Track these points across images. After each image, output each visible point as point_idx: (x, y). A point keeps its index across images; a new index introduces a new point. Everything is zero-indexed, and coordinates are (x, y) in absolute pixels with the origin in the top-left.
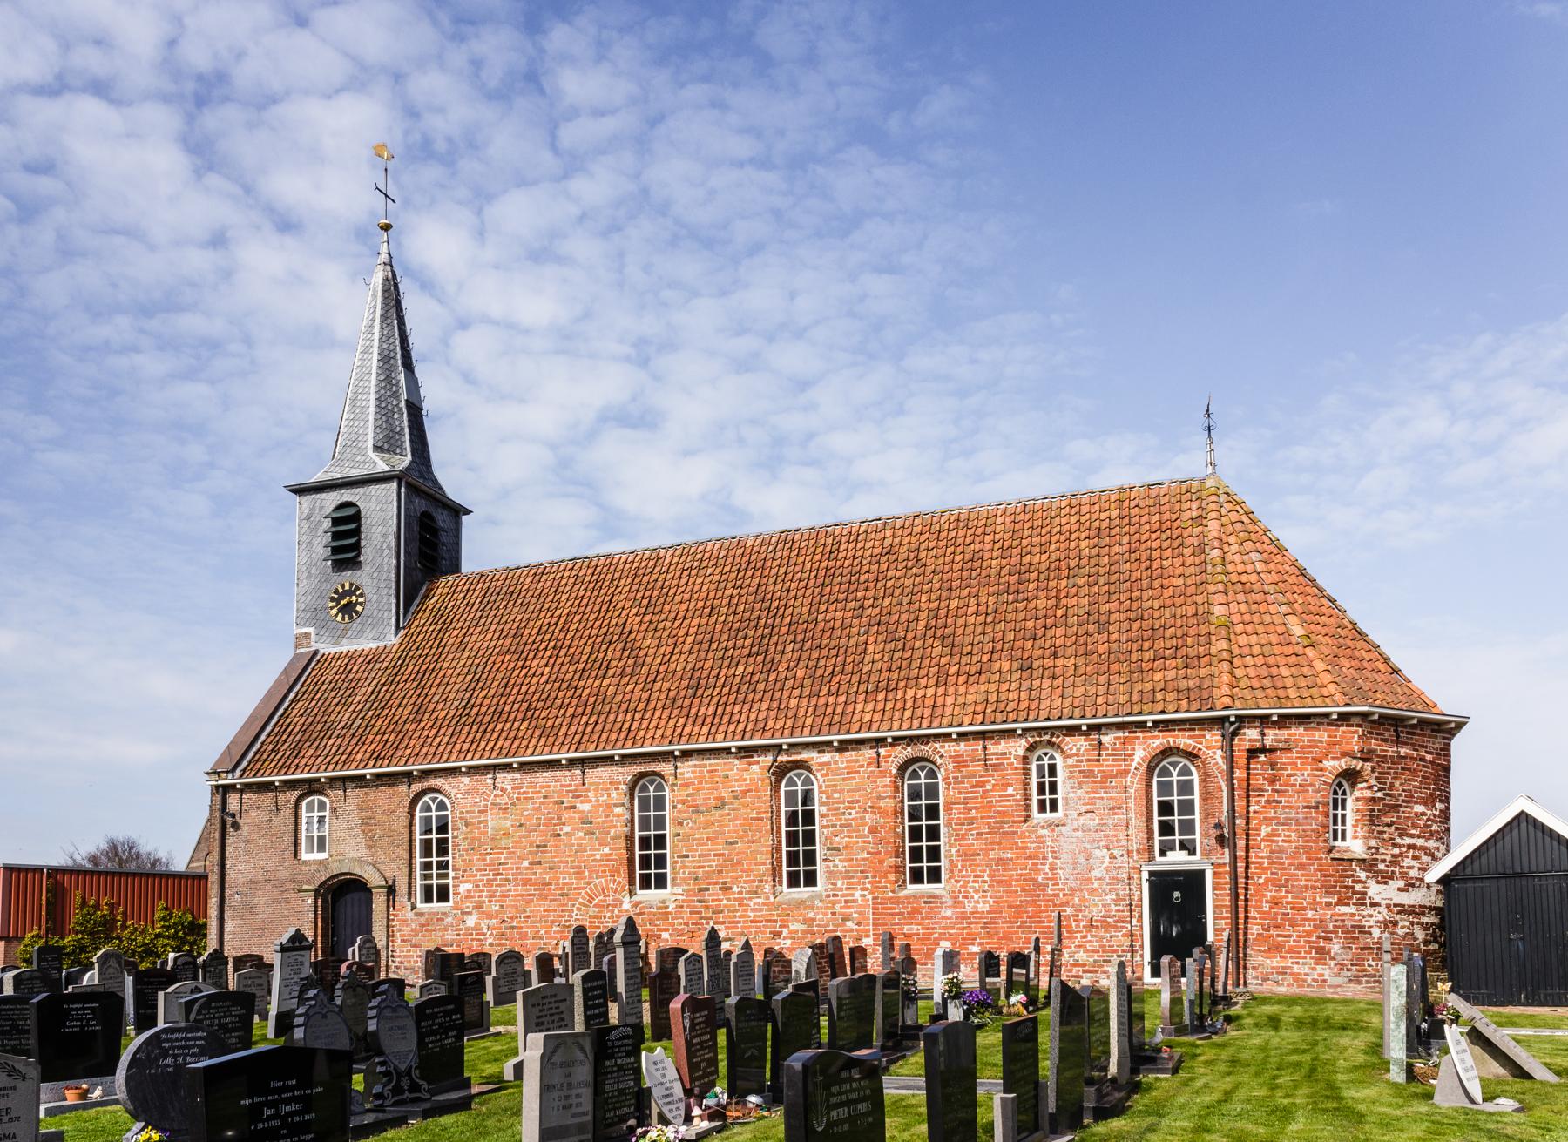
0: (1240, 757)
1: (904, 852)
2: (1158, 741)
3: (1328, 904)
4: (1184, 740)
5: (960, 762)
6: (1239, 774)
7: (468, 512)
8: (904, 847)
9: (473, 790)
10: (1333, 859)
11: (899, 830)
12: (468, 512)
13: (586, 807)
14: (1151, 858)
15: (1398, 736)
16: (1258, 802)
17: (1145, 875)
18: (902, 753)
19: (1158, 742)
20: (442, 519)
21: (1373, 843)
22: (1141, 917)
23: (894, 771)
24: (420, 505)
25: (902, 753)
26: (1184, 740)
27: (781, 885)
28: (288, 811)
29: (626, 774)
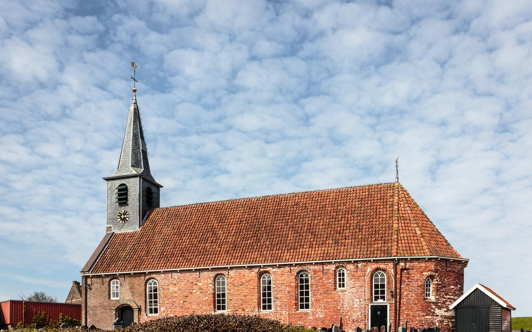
0: (398, 271)
1: (298, 299)
2: (374, 266)
3: (423, 315)
4: (382, 266)
5: (315, 272)
6: (398, 276)
7: (162, 187)
8: (298, 298)
9: (165, 278)
10: (425, 302)
11: (297, 292)
12: (162, 187)
13: (200, 284)
14: (372, 301)
15: (446, 265)
16: (404, 285)
17: (370, 307)
18: (298, 269)
19: (374, 266)
20: (154, 189)
21: (437, 297)
22: (368, 319)
23: (295, 274)
24: (147, 185)
25: (298, 269)
26: (382, 266)
27: (261, 309)
28: (106, 284)
29: (213, 274)
